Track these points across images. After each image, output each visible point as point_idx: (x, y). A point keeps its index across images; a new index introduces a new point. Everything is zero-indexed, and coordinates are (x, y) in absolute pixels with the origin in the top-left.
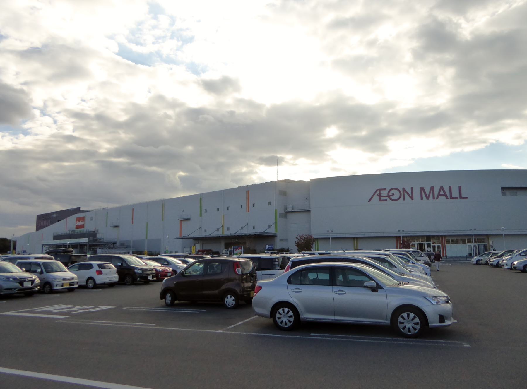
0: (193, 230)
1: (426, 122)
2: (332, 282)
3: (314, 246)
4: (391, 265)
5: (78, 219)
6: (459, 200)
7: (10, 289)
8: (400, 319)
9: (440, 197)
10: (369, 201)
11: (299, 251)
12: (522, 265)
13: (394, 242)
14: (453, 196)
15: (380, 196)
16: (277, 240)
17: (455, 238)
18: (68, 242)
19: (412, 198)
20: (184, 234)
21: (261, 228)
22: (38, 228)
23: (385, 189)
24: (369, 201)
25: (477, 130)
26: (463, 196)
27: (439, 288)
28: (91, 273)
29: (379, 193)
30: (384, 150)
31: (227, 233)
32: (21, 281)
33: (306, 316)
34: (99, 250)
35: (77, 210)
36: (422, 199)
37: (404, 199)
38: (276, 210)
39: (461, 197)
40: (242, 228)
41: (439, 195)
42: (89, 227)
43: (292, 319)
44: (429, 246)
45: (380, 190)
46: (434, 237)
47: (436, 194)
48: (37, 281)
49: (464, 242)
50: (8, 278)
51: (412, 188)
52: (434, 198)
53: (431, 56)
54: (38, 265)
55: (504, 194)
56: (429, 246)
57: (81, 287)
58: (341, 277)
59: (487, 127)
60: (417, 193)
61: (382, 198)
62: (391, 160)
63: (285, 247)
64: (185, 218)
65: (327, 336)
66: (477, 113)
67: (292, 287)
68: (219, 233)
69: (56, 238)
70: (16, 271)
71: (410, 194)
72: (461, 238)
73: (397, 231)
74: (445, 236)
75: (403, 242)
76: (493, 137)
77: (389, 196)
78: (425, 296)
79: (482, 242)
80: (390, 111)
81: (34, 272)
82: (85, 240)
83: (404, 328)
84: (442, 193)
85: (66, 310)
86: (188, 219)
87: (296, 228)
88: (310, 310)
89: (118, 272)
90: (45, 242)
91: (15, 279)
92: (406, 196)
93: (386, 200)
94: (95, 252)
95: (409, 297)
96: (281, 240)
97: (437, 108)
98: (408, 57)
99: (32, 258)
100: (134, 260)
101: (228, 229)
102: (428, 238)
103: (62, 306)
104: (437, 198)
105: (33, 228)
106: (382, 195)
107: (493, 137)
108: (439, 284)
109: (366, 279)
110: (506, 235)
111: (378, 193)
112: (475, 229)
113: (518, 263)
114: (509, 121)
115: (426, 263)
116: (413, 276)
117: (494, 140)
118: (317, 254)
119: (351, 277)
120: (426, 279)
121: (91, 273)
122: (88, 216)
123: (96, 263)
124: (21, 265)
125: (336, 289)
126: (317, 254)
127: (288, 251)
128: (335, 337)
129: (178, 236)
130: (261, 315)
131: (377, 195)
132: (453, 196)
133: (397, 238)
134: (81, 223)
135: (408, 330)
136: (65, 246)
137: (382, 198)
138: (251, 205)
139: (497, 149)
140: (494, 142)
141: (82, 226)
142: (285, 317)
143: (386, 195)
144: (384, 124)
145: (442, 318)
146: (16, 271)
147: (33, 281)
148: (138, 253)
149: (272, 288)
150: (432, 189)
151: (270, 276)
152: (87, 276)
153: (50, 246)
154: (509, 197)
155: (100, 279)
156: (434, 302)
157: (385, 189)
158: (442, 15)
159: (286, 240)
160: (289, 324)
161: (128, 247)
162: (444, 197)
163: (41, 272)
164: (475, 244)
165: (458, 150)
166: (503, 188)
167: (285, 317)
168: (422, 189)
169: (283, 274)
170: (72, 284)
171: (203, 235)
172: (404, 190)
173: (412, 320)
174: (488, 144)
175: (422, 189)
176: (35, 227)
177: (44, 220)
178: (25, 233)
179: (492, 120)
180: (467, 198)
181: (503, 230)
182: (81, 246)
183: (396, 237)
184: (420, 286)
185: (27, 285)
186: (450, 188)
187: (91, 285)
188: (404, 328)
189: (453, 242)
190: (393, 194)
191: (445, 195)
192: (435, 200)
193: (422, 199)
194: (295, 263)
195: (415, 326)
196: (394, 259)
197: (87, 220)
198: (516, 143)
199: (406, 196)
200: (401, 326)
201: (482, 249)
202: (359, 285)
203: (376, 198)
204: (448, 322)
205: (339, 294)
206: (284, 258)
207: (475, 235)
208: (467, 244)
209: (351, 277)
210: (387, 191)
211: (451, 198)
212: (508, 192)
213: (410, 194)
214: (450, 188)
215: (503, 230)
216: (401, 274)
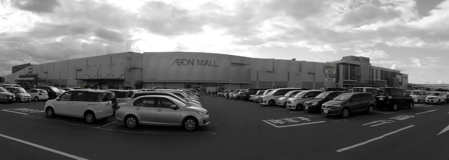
0: (82, 75)
2: (155, 105)
3: (144, 86)
4: (182, 97)
5: (30, 69)
6: (214, 67)
7: (4, 99)
8: (186, 123)
11: (137, 89)
13: (183, 85)
15: (177, 63)
16: (125, 82)
18: (25, 79)
20: (79, 77)
21: (117, 76)
22: (13, 72)
27: (204, 108)
28: (37, 94)
31: (100, 78)
32: (8, 96)
34: (39, 84)
35: (29, 65)
38: (125, 67)
40: (107, 76)
41: (205, 64)
42: (34, 72)
43: (135, 123)
44: (199, 87)
46: (201, 83)
47: (204, 63)
48: (14, 96)
49: (214, 86)
50: (3, 95)
54: (14, 89)
55: (232, 66)
56: (199, 87)
57: (32, 100)
58: (159, 103)
63: (129, 86)
64: (78, 69)
67: (135, 107)
68: (96, 78)
69: (20, 77)
70: (7, 92)
75: (188, 85)
77: (182, 63)
78: (198, 111)
79: (221, 86)
81: (13, 92)
82: (32, 79)
83: (188, 127)
85: (27, 111)
86: (80, 70)
87: (136, 77)
89: (48, 94)
90: (15, 79)
91: (6, 95)
94: (37, 85)
95: (191, 112)
96: (127, 82)
99: (13, 85)
100: (55, 89)
101: (100, 76)
102: (199, 84)
103: (25, 109)
105: (10, 72)
108: (204, 106)
109: (171, 103)
110: (231, 84)
115: (197, 96)
116: (193, 102)
118: (146, 91)
119: (164, 103)
120: (198, 103)
121: (37, 94)
122: (34, 67)
123: (38, 90)
124: (8, 89)
125: (157, 109)
126: (146, 91)
127: (131, 88)
129: (75, 78)
130: (118, 121)
133: (185, 83)
134: (31, 70)
135: (189, 127)
136: (24, 81)
138: (112, 64)
141: (31, 72)
145: (205, 122)
146: (7, 92)
147: (13, 96)
148: (56, 86)
151: (123, 101)
152: (35, 96)
153: (18, 80)
155: (41, 97)
156: (202, 114)
159: (130, 83)
160: (133, 126)
161: (51, 83)
163: (16, 93)
167: (131, 122)
169: (130, 100)
170: (29, 99)
171: (87, 78)
172: (189, 60)
175: (198, 60)
176: (11, 71)
177: (16, 69)
182: (31, 81)
183: (184, 83)
184: (196, 107)
185: (10, 98)
187: (36, 100)
188: (188, 127)
189: (210, 86)
191: (208, 64)
194: (137, 95)
196: (184, 94)
197: (34, 69)
200: (186, 126)
201: (221, 89)
202: (168, 106)
203: (176, 64)
204: (207, 124)
206: (130, 92)
209: (164, 103)
211: (211, 66)
216: (187, 101)
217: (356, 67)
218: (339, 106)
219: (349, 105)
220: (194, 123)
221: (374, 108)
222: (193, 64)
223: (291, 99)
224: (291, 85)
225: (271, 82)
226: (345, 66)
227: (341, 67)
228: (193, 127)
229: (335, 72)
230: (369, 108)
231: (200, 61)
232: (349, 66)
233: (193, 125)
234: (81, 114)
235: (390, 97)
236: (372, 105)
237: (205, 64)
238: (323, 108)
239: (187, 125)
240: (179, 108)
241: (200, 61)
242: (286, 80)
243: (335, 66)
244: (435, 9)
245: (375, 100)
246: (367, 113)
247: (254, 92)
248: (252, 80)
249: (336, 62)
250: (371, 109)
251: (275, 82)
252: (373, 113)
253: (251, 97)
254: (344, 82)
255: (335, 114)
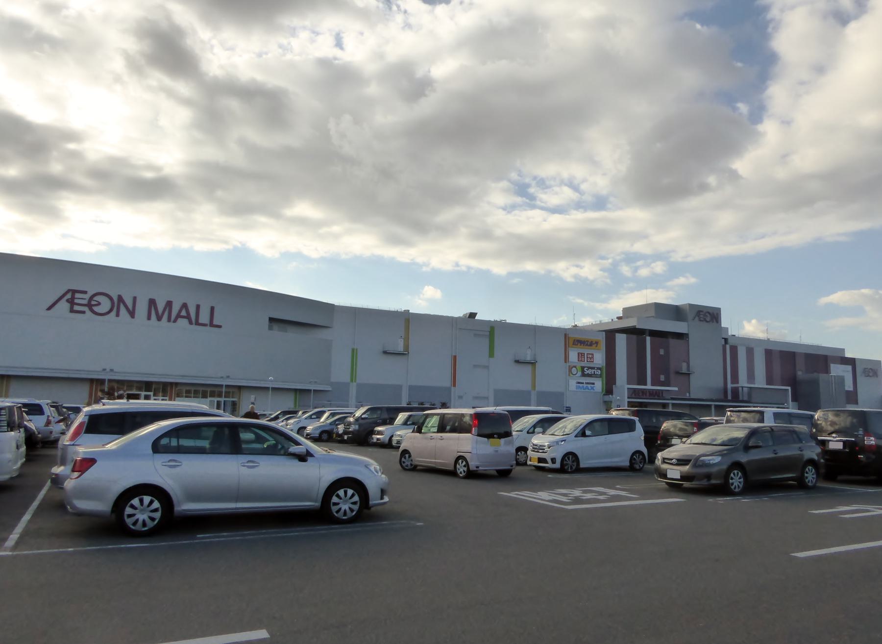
1: (146, 188)
6: (208, 328)
9: (180, 320)
10: (49, 308)
12: (318, 432)
14: (200, 321)
15: (71, 302)
17: (193, 389)
19: (132, 314)
23: (85, 292)
24: (49, 308)
25: (218, 220)
26: (215, 323)
29: (71, 297)
30: (53, 214)
33: (185, 506)
36: (149, 318)
37: (118, 315)
39: (212, 325)
41: (179, 316)
45: (74, 292)
51: (135, 299)
52: (169, 320)
53: (158, 77)
55: (270, 328)
59: (233, 220)
60: (142, 309)
61: (76, 308)
62: (64, 236)
65: (225, 536)
66: (220, 193)
71: (130, 307)
72: (201, 389)
73: (100, 369)
74: (177, 384)
76: (238, 237)
77: (89, 306)
80: (72, 146)
84: (184, 313)
88: (194, 496)
92: (123, 310)
93: (84, 312)
97: (157, 169)
98: (118, 64)
104: (175, 321)
106: (76, 301)
107: (238, 237)
110: (274, 389)
111: (69, 296)
112: (228, 377)
113: (315, 429)
114: (262, 219)
117: (240, 243)
128: (219, 537)
131: (68, 301)
132: (200, 321)
137: (76, 308)
139: (242, 254)
140: (239, 245)
142: (143, 512)
143: (85, 302)
144: (56, 168)
149: (116, 465)
150: (169, 304)
154: (279, 335)
157: (85, 292)
158: (184, 16)
160: (151, 524)
162: (186, 321)
164: (219, 399)
165: (185, 245)
166: (272, 320)
168: (152, 303)
172: (120, 299)
173: (351, 498)
174: (230, 247)
175: (152, 303)
178: (821, 390)
179: (241, 210)
180: (220, 327)
181: (271, 381)
186: (198, 307)
190: (99, 304)
191: (188, 317)
192: (171, 324)
193: (149, 318)
195: (353, 507)
198: (269, 253)
199: (123, 310)
200: (334, 509)
203: (64, 305)
205: (249, 467)
207: (227, 386)
208: (209, 399)
210: (87, 296)
211: (197, 323)
212: (275, 326)
213: (130, 307)
214: (198, 307)
215: (271, 381)
217: (673, 342)
218: (717, 459)
219: (743, 458)
220: (356, 498)
221: (818, 473)
222: (132, 314)
223: (538, 439)
224: (460, 397)
225: (399, 388)
226: (634, 337)
227: (621, 341)
228: (352, 510)
229: (599, 358)
230: (803, 471)
231: (161, 306)
232: (648, 339)
233: (355, 503)
234: (446, 461)
235: (871, 441)
236: (811, 462)
237: (179, 316)
238: (665, 466)
239: (335, 504)
240: (312, 455)
241: (161, 306)
242: (446, 382)
243: (602, 338)
244: (277, 216)
245: (819, 450)
246: (801, 485)
247: (385, 416)
248: (333, 380)
249: (601, 324)
250: (810, 475)
251: (412, 388)
252: (814, 488)
253: (380, 433)
254: (634, 393)
255: (705, 483)
